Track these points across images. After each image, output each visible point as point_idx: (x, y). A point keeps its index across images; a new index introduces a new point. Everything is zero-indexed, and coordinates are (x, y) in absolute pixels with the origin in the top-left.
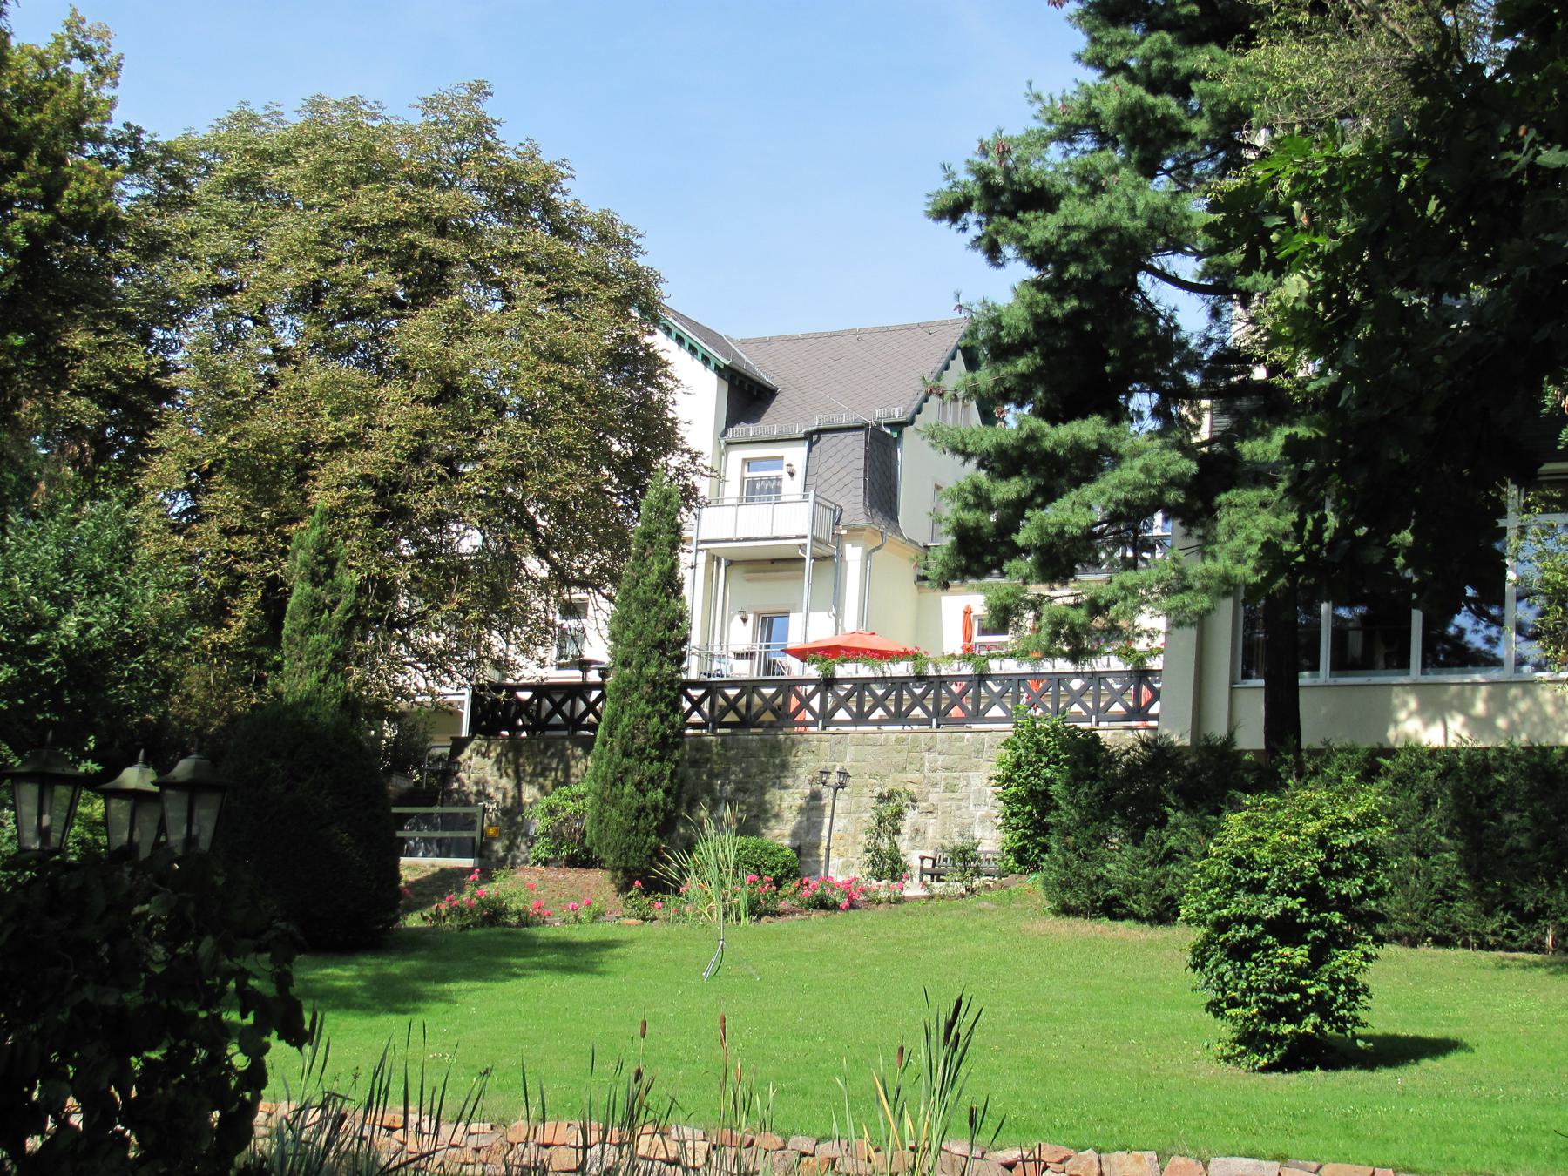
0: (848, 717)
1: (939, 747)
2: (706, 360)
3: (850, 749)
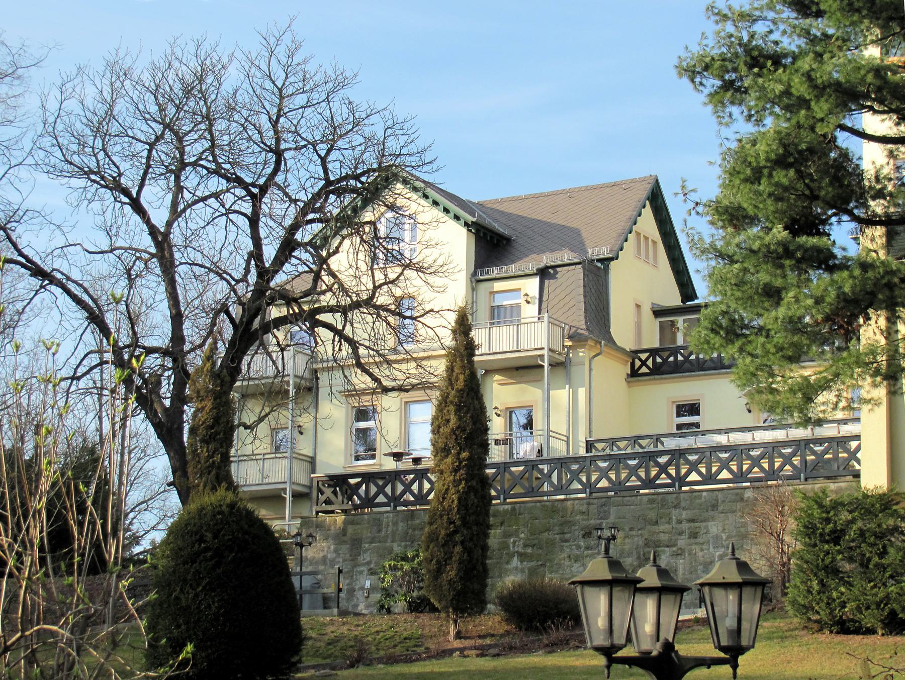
0: (699, 478)
1: (683, 504)
2: (457, 218)
3: (613, 510)
